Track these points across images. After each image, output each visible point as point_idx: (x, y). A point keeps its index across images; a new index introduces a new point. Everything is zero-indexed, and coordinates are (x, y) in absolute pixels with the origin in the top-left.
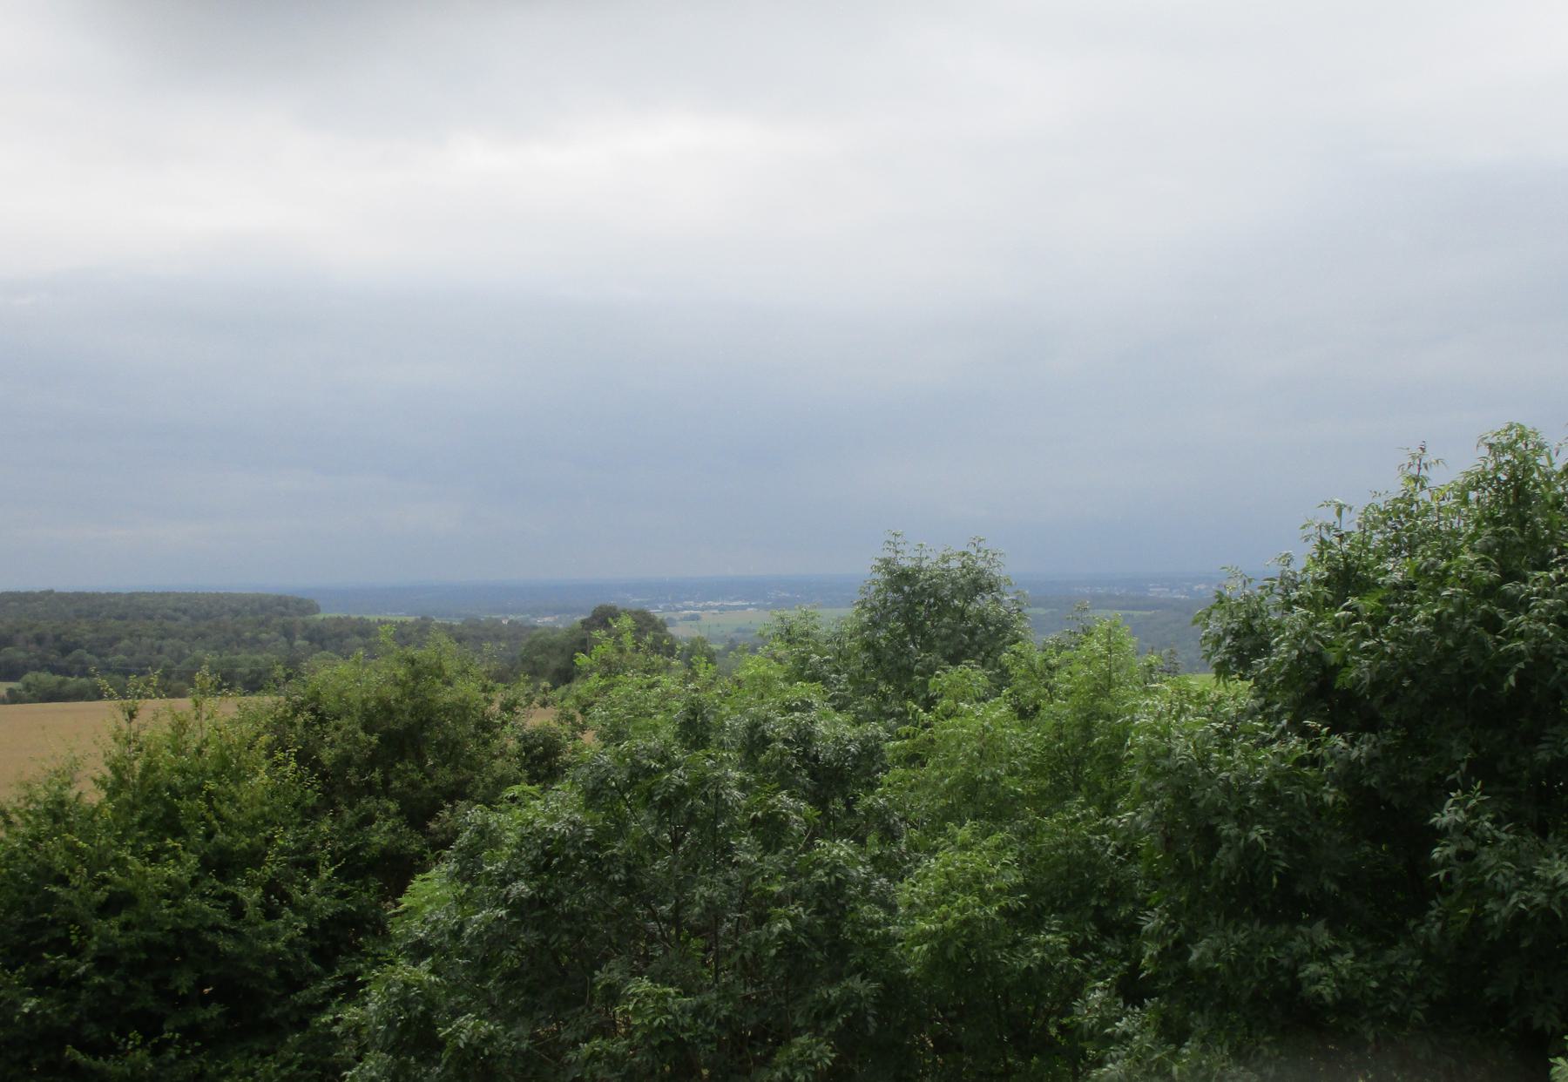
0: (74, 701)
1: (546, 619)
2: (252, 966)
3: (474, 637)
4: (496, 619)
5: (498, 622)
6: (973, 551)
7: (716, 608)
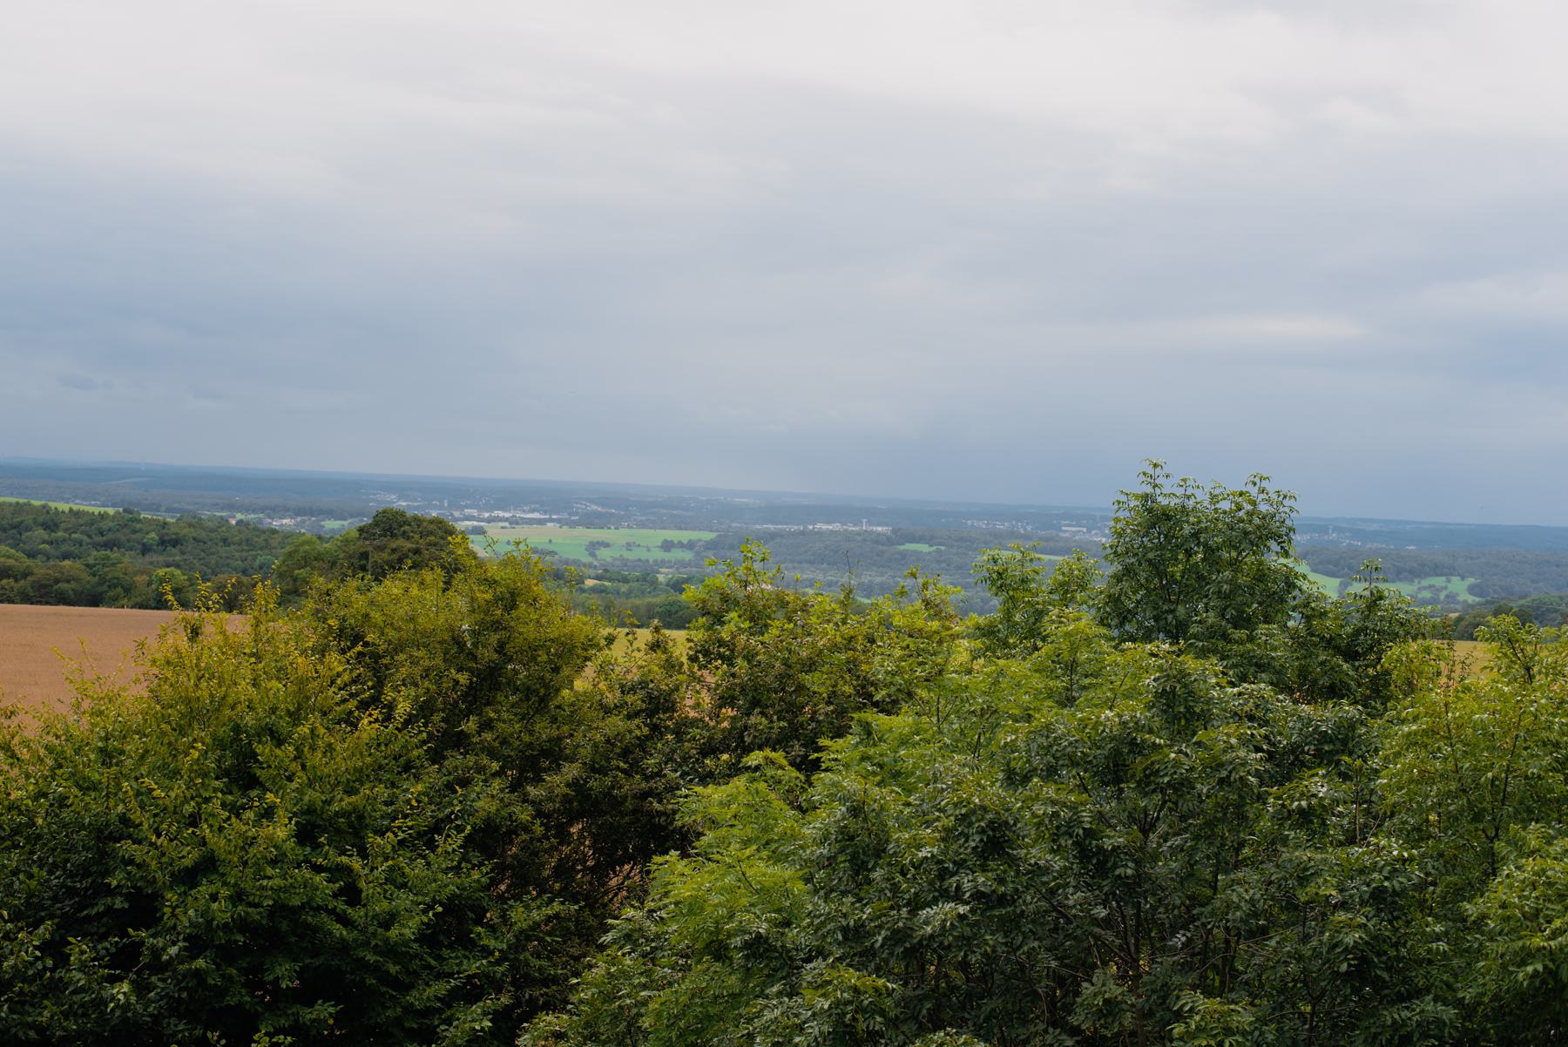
0: (86, 606)
1: (284, 521)
2: (371, 958)
3: (194, 539)
4: (221, 517)
5: (224, 521)
6: (1254, 491)
7: (506, 520)
